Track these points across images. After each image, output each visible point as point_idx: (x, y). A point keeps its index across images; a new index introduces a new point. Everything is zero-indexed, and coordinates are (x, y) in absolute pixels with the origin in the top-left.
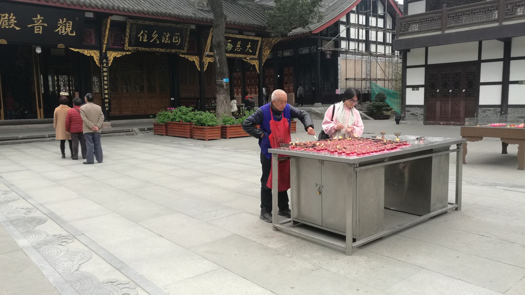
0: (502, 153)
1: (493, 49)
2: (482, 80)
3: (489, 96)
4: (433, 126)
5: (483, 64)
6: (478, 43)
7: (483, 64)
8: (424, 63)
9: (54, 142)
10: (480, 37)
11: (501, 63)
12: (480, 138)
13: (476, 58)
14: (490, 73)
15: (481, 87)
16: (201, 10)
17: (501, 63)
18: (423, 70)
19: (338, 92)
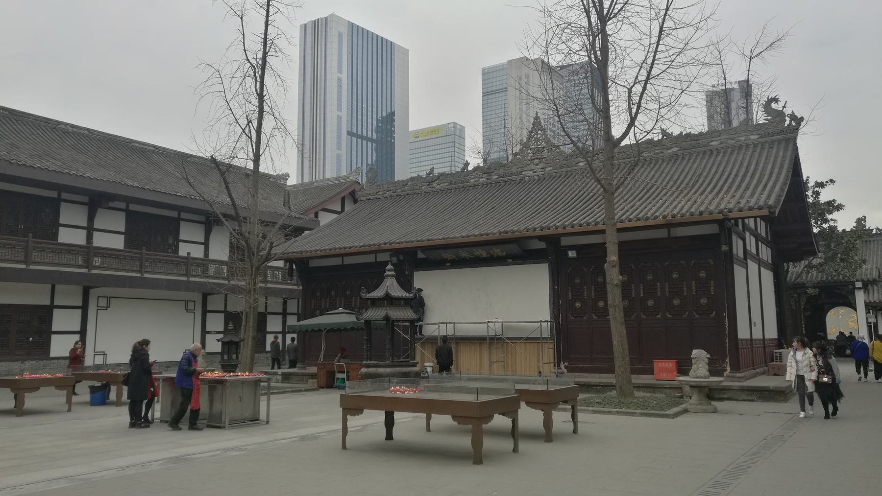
0: (386, 439)
1: (69, 295)
2: (54, 328)
3: (60, 346)
4: (314, 392)
5: (56, 311)
6: (50, 286)
7: (56, 311)
8: (223, 309)
9: (714, 416)
10: (53, 281)
11: (79, 311)
12: (37, 389)
13: (48, 303)
14: (64, 320)
15: (53, 337)
16: (622, 183)
17: (79, 311)
18: (222, 316)
19: (833, 360)
